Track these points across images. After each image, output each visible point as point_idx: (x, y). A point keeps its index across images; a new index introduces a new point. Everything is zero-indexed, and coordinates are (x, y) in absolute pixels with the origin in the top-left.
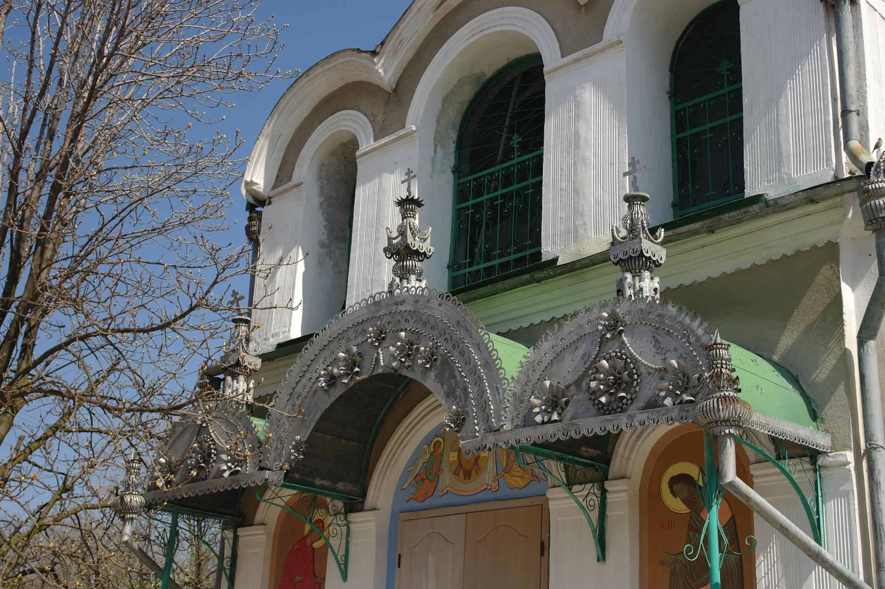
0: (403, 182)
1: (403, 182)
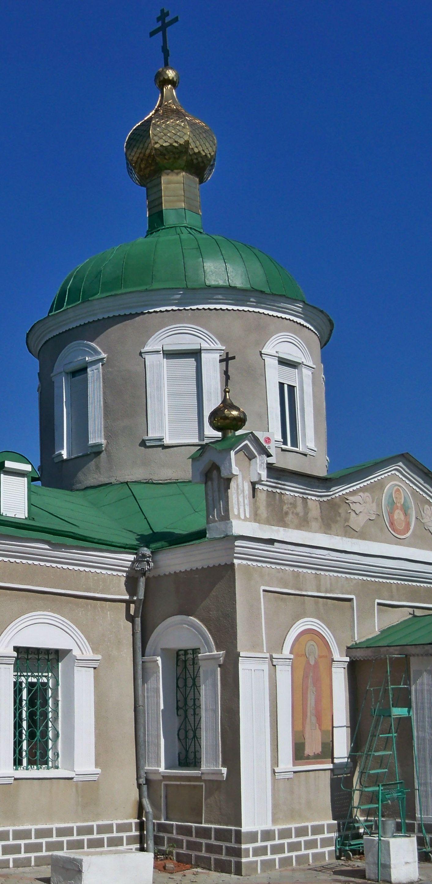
0: (152, 34)
1: (152, 34)
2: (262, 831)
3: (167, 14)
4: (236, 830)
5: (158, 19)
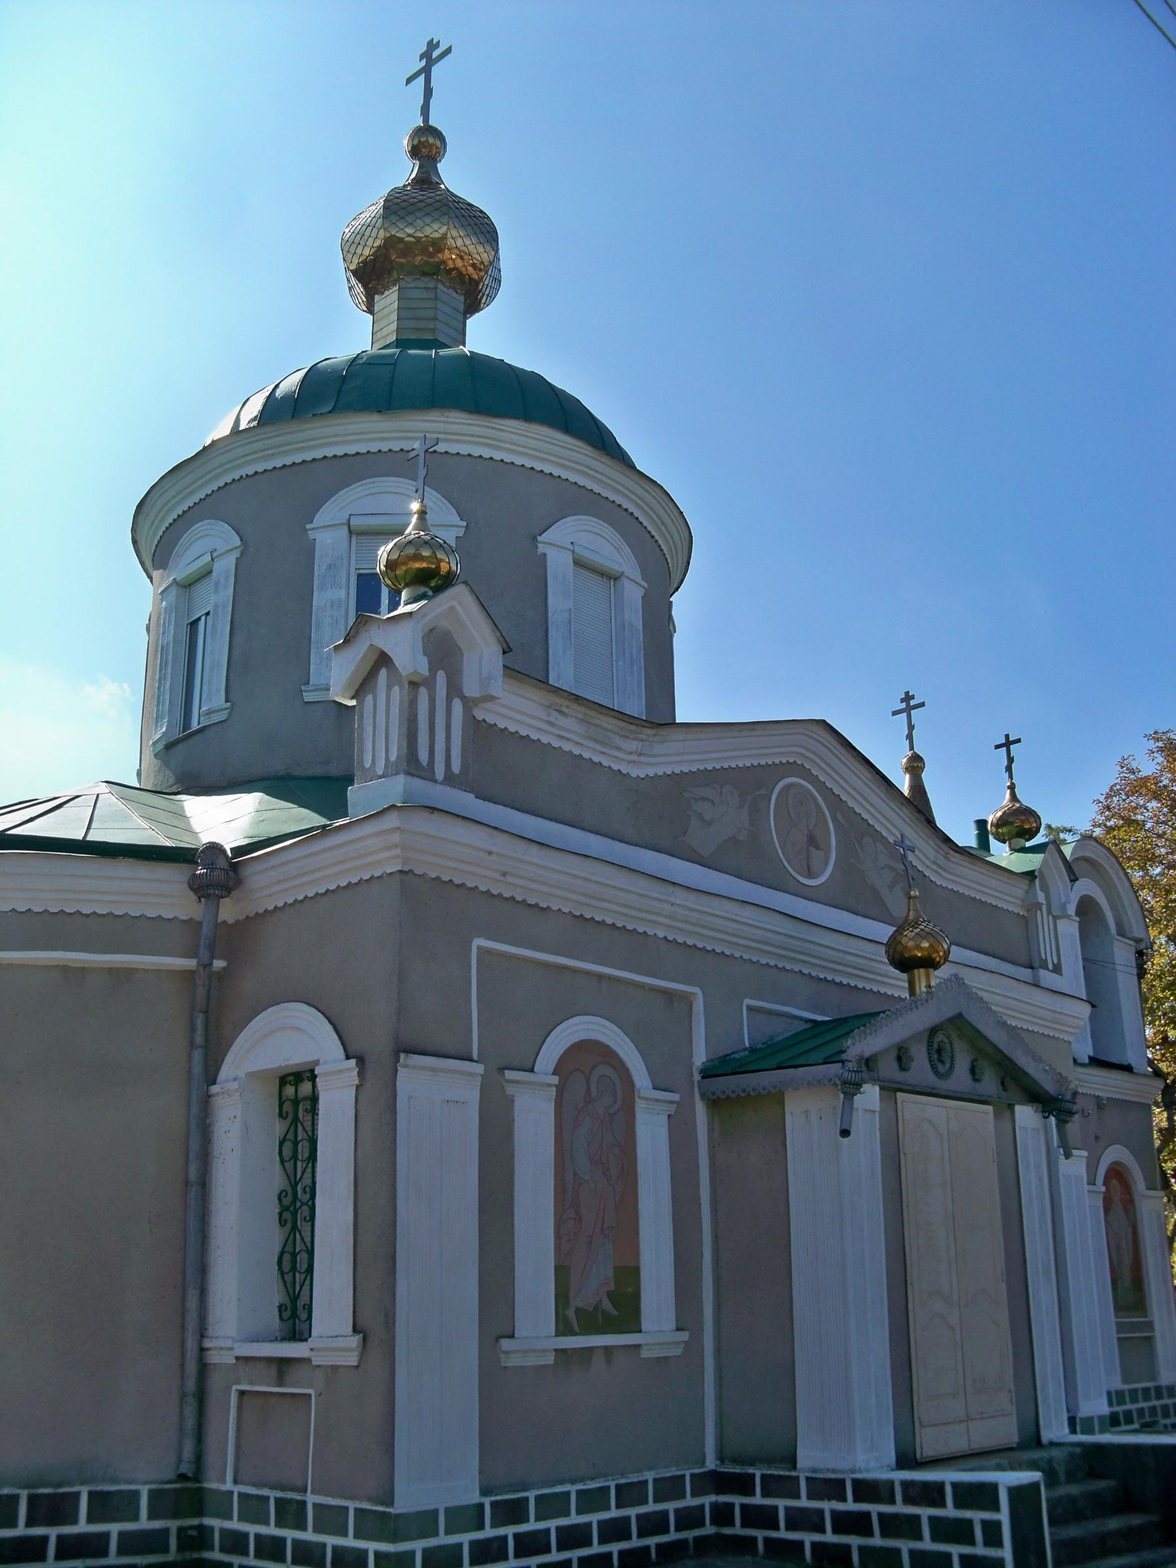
2: (447, 1510)
3: (913, 697)
4: (985, 1524)
5: (902, 701)
